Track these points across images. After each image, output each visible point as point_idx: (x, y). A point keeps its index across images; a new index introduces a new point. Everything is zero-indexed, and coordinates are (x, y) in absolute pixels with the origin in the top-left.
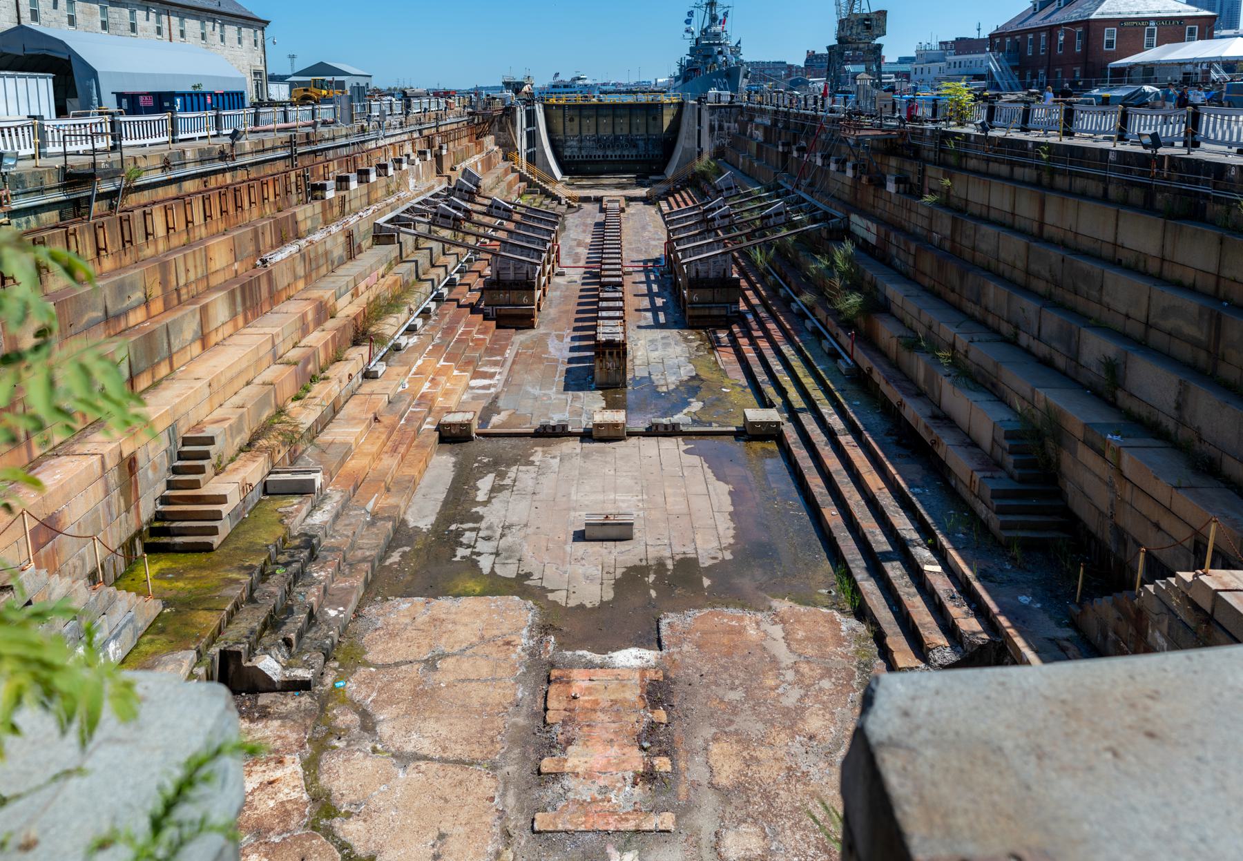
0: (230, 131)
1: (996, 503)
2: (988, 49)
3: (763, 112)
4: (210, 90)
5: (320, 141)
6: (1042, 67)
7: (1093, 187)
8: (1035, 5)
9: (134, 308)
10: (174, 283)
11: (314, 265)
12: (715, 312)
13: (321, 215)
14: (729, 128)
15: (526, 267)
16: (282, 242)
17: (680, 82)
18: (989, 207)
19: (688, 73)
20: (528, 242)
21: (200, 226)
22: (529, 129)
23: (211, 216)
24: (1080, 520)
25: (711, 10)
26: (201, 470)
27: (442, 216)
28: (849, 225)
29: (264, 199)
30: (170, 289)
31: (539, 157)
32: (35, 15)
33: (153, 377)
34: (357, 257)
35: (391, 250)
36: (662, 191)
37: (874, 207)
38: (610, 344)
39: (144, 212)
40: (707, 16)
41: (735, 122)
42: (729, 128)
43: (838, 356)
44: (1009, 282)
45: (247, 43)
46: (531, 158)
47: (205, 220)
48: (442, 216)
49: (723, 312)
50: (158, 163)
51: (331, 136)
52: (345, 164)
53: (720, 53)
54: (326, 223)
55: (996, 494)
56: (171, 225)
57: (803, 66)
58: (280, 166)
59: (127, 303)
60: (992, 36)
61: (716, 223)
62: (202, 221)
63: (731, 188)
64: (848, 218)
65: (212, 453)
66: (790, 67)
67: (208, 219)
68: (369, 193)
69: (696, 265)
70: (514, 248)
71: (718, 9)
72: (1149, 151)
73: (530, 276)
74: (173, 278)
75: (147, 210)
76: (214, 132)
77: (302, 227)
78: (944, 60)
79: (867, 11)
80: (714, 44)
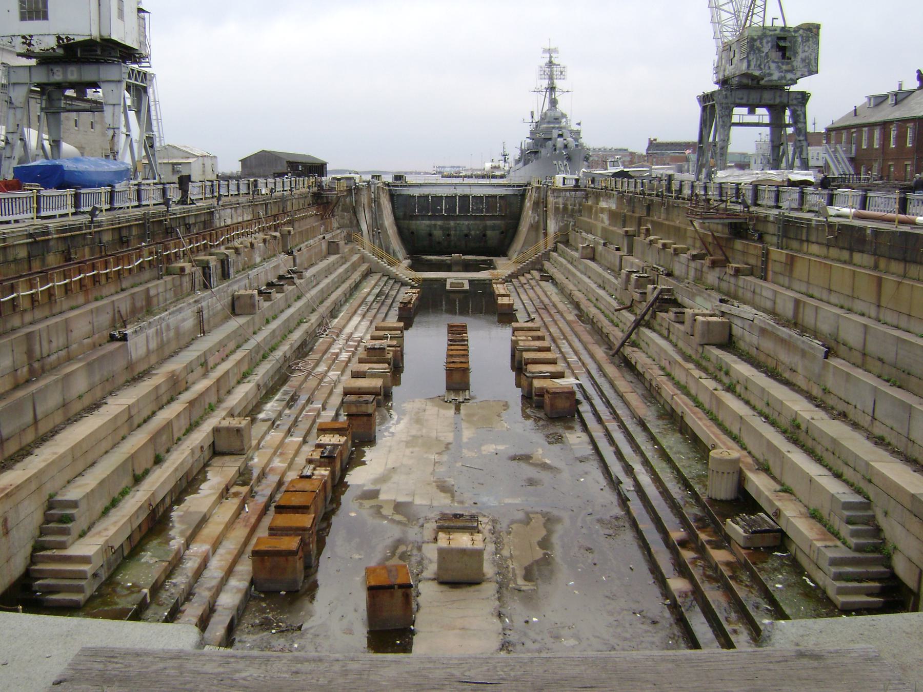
0: (89, 209)
1: (833, 570)
2: (824, 142)
6: (875, 160)
17: (521, 164)
19: (529, 155)
24: (635, 153)
25: (551, 94)
26: (65, 532)
34: (866, 100)
40: (547, 100)
53: (560, 136)
55: (834, 562)
57: (645, 153)
60: (829, 130)
65: (76, 516)
66: (632, 154)
74: (37, 347)
76: (136, 204)
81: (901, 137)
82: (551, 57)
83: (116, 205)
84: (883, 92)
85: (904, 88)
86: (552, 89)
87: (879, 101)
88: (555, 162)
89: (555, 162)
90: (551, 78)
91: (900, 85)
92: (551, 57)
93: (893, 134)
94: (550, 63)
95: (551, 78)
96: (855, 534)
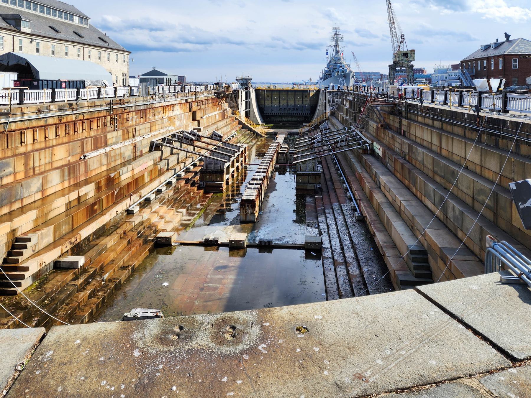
3: (350, 94)
4: (79, 80)
5: (128, 103)
7: (460, 131)
8: (482, 47)
9: (7, 176)
10: (32, 165)
11: (113, 159)
12: (309, 187)
13: (121, 137)
14: (337, 101)
15: (220, 163)
16: (96, 148)
17: (323, 80)
18: (423, 139)
19: (327, 75)
20: (227, 152)
21: (53, 139)
22: (246, 100)
23: (59, 135)
27: (185, 138)
28: (373, 147)
29: (91, 128)
30: (29, 167)
31: (251, 113)
32: (21, 48)
33: (10, 208)
35: (158, 154)
36: (306, 131)
37: (383, 139)
38: (248, 201)
39: (21, 132)
40: (335, 51)
41: (340, 99)
42: (337, 101)
43: (356, 210)
44: (426, 176)
45: (120, 61)
46: (248, 115)
47: (56, 137)
48: (185, 138)
49: (313, 188)
50: (35, 110)
51: (134, 101)
52: (139, 114)
54: (124, 140)
56: (35, 138)
58: (104, 113)
59: (3, 173)
61: (315, 145)
62: (54, 137)
63: (327, 129)
64: (373, 144)
67: (58, 136)
68: (150, 127)
69: (300, 165)
70: (218, 154)
71: (339, 48)
72: (476, 114)
73: (222, 168)
75: (23, 131)
77: (109, 142)
78: (447, 73)
79: (406, 50)
80: (338, 63)
81: (496, 64)
82: (336, 31)
83: (101, 97)
84: (488, 43)
85: (499, 41)
86: (337, 45)
87: (487, 48)
88: (338, 79)
89: (338, 79)
90: (336, 41)
91: (497, 40)
92: (336, 31)
93: (485, 62)
94: (336, 34)
95: (336, 41)
96: (416, 268)
